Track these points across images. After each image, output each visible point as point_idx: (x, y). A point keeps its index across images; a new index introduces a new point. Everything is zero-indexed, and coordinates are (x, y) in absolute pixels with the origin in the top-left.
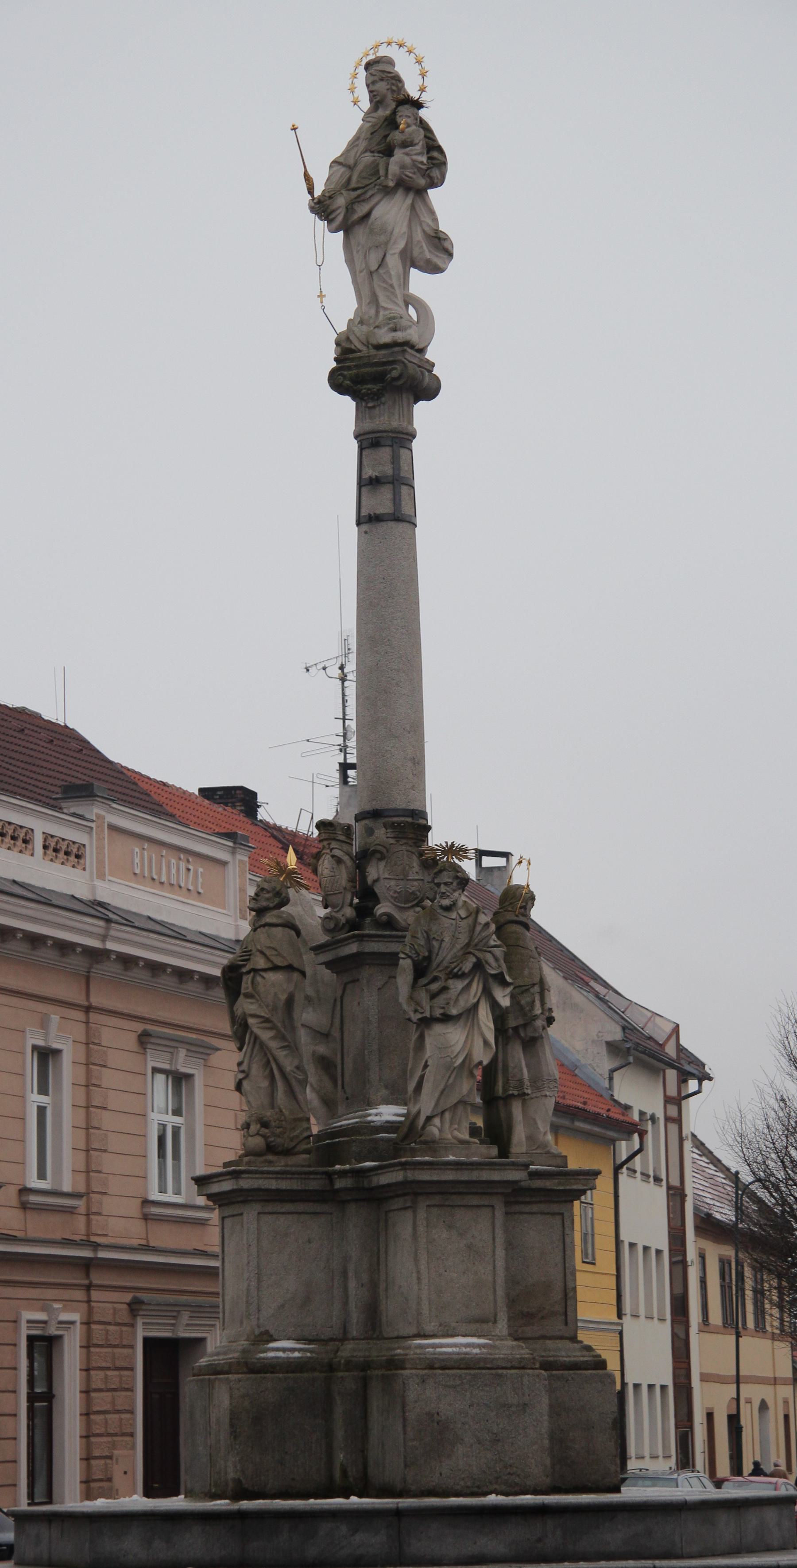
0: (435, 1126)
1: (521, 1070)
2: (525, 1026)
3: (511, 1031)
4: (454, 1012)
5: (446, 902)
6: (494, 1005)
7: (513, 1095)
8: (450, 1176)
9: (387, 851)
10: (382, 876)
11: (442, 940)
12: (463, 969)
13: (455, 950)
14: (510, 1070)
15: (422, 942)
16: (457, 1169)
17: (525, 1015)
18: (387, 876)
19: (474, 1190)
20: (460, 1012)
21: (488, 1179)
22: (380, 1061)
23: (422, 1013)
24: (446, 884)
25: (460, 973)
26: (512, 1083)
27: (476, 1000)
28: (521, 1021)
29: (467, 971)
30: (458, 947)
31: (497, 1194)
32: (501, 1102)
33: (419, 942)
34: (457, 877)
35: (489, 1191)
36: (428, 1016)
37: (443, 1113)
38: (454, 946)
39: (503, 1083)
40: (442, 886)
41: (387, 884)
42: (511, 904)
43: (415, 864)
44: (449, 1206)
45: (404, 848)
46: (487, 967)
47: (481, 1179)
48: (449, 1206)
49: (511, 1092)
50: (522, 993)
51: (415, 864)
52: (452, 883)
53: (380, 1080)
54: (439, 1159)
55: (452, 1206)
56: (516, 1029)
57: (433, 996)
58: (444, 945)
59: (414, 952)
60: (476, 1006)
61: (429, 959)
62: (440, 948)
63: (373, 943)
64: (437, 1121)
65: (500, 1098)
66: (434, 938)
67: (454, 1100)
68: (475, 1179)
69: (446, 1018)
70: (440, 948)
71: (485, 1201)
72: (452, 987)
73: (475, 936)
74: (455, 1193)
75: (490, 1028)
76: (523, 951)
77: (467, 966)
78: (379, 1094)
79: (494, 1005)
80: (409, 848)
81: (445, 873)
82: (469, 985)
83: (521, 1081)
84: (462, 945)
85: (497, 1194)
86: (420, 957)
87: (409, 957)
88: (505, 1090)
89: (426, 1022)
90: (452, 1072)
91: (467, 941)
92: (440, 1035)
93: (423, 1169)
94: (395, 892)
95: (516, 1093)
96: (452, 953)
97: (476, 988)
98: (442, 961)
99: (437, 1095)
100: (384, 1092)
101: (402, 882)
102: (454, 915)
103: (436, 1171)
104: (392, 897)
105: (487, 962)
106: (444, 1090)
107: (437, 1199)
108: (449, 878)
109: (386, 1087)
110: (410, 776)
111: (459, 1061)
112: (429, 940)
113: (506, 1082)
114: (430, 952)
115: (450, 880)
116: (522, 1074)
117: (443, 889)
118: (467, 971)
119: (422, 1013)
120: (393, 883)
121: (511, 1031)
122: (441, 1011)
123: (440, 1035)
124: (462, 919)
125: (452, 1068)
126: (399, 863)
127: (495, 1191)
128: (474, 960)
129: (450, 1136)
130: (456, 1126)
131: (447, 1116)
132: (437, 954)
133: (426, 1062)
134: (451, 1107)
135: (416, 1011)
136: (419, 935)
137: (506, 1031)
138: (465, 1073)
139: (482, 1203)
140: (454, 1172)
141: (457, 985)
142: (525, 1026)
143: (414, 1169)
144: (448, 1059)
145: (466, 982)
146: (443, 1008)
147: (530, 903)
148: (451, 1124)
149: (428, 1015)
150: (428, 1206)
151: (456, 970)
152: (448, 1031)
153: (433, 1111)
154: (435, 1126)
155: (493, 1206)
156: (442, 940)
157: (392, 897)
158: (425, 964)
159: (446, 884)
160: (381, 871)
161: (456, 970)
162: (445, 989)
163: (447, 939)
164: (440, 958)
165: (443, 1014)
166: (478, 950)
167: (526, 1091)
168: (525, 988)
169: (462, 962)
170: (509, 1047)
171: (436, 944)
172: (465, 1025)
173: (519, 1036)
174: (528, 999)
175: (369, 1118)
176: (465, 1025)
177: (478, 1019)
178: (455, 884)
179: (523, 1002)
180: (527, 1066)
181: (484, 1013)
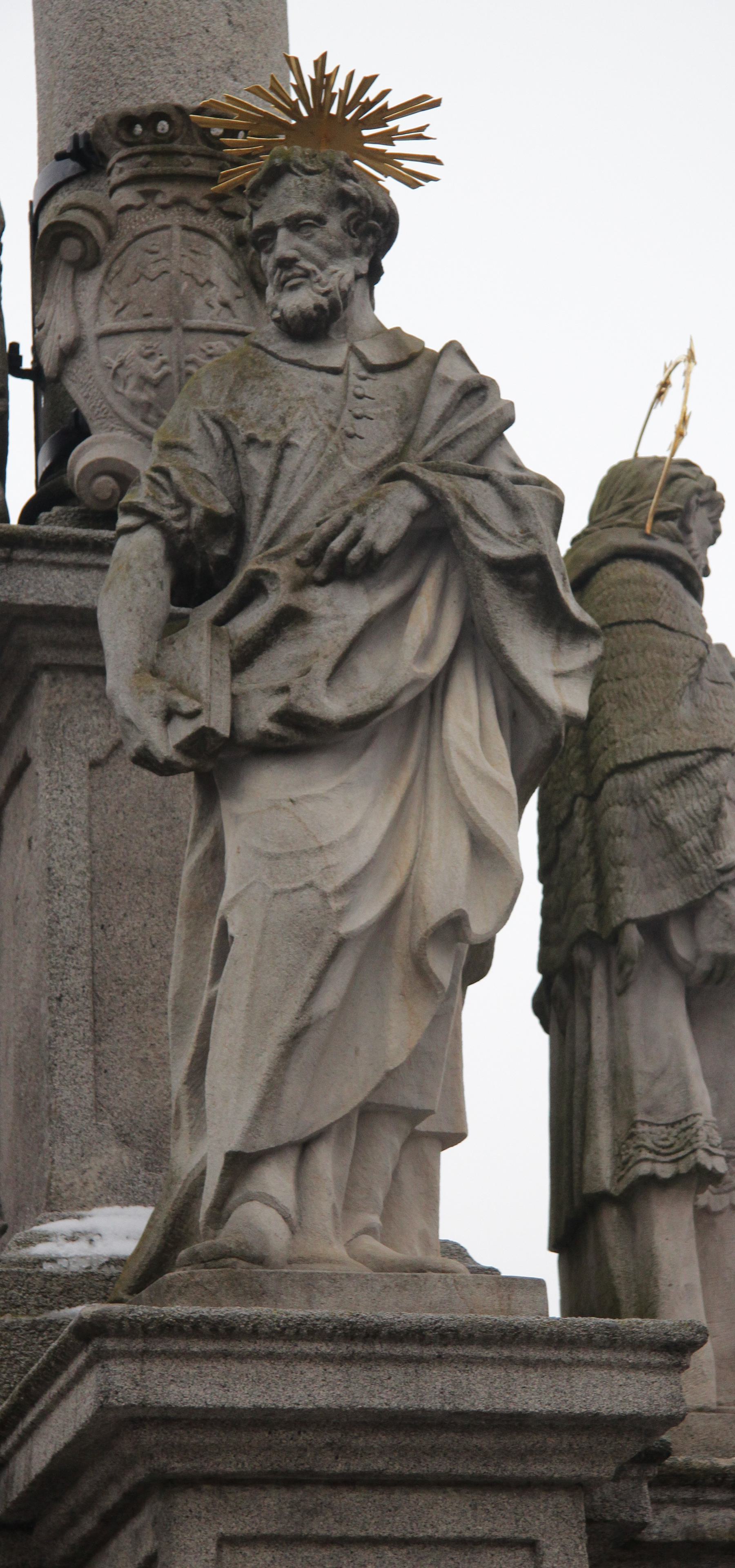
0: (269, 1201)
1: (684, 1084)
2: (690, 913)
3: (633, 937)
4: (334, 706)
5: (301, 300)
6: (517, 703)
7: (652, 1181)
8: (314, 1387)
9: (110, 234)
10: (91, 331)
11: (286, 445)
12: (368, 536)
13: (339, 480)
14: (640, 1083)
15: (205, 462)
16: (349, 1359)
17: (687, 868)
18: (110, 324)
19: (440, 1466)
20: (362, 707)
21: (500, 1405)
22: (97, 1039)
23: (193, 715)
24: (296, 224)
25: (355, 553)
26: (649, 1136)
27: (431, 668)
28: (673, 898)
29: (383, 544)
30: (355, 467)
31: (550, 1485)
32: (610, 1217)
33: (192, 461)
34: (343, 199)
35: (513, 1469)
36: (224, 729)
37: (304, 1147)
38: (332, 463)
39: (615, 1140)
40: (282, 233)
41: (112, 352)
42: (627, 508)
43: (216, 274)
44: (326, 1542)
45: (173, 217)
46: (471, 526)
47: (465, 1405)
48: (326, 1542)
49: (645, 1169)
50: (672, 780)
51: (216, 274)
52: (320, 220)
53: (99, 1107)
54: (263, 1310)
55: (343, 1542)
56: (655, 929)
57: (244, 658)
58: (292, 460)
59: (168, 499)
60: (435, 692)
61: (232, 527)
62: (275, 476)
63: (57, 575)
64: (275, 1179)
65: (604, 1197)
66: (251, 440)
67: (346, 1092)
68: (432, 1403)
69: (301, 737)
70: (275, 476)
71: (496, 1517)
72: (323, 610)
73: (424, 431)
74: (350, 1481)
75: (496, 786)
76: (668, 639)
77: (389, 520)
78: (95, 1164)
79: (517, 703)
80: (199, 221)
81: (290, 181)
82: (403, 605)
83: (684, 1125)
84: (369, 463)
85: (550, 1485)
86: (196, 514)
87: (152, 519)
88: (622, 1163)
89: (215, 763)
90: (333, 957)
91: (390, 447)
92: (276, 806)
93: (188, 1356)
94: (144, 381)
95: (665, 1171)
96: (327, 490)
97: (430, 625)
98: (285, 525)
99: (267, 1057)
100: (113, 1157)
101: (163, 342)
102: (335, 354)
103: (250, 1369)
104: (134, 405)
105: (470, 509)
106: (295, 1038)
107: (269, 1511)
108: (307, 196)
109: (125, 1140)
110: (220, 26)
111: (365, 913)
112: (231, 451)
113: (627, 1137)
114: (241, 500)
115: (313, 208)
116: (688, 1095)
117: (285, 244)
118: (383, 544)
119: (193, 715)
120: (132, 346)
121: (633, 937)
122: (277, 703)
123: (276, 806)
124: (374, 369)
125: (328, 941)
126: (154, 270)
127: (538, 1469)
128: (417, 499)
129: (338, 1250)
130: (375, 1219)
131: (325, 1161)
132: (267, 503)
133: (224, 926)
134: (344, 1122)
135: (170, 714)
136: (194, 438)
137: (616, 936)
138: (397, 973)
139: (482, 1529)
140: (335, 1374)
141: (343, 610)
142: (690, 913)
143: (144, 1355)
144: (309, 898)
145: (387, 596)
146: (284, 689)
147: (699, 520)
148: (349, 1203)
149: (220, 722)
150: (224, 1541)
151: (337, 545)
152: (319, 789)
153: (252, 1130)
154: (269, 1201)
155: (532, 1545)
156: (286, 445)
157: (134, 405)
158: (220, 551)
159: (296, 224)
160: (87, 315)
161: (337, 545)
162: (290, 619)
163: (303, 440)
164: (278, 513)
165: (287, 717)
166: (434, 469)
167: (709, 1163)
168: (679, 762)
169: (361, 508)
170: (633, 1000)
171: (259, 463)
172: (392, 774)
173: (668, 957)
174: (696, 805)
175: (41, 1249)
176: (392, 774)
177: (446, 768)
178: (334, 224)
179: (673, 817)
180: (715, 1082)
181: (472, 727)
